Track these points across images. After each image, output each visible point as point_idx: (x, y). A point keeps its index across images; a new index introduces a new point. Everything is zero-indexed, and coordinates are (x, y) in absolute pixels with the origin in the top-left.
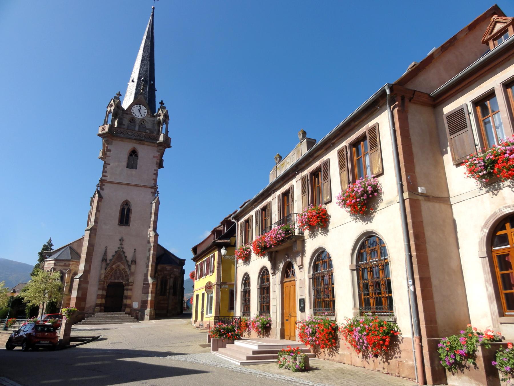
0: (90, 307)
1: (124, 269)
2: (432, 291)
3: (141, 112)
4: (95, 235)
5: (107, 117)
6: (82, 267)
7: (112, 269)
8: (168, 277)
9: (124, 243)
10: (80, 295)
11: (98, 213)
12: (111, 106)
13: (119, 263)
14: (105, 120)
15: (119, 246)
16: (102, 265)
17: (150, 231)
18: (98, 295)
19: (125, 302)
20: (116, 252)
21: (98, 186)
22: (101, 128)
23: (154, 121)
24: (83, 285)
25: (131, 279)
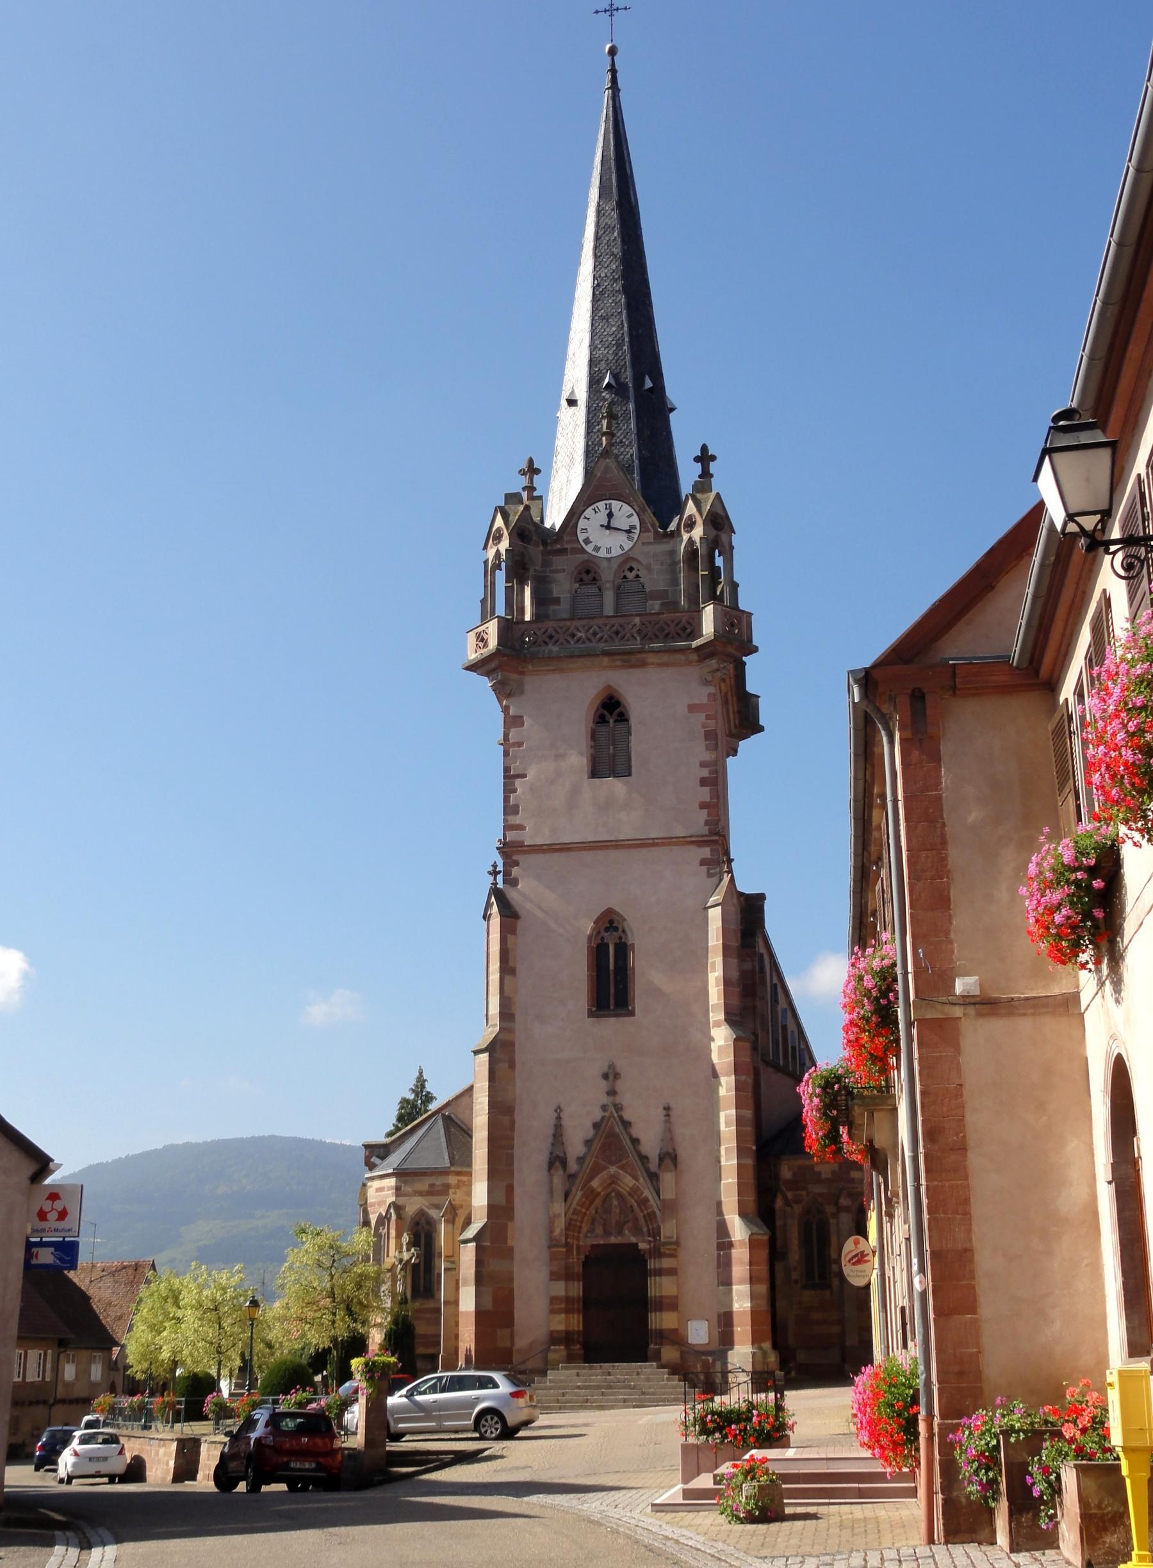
0: (531, 1345)
1: (634, 1191)
2: (973, 1287)
3: (612, 535)
4: (512, 1066)
5: (490, 587)
6: (480, 1194)
7: (591, 1195)
8: (829, 1209)
9: (620, 1086)
10: (488, 1305)
11: (508, 978)
12: (498, 538)
13: (613, 1169)
14: (484, 601)
15: (605, 1099)
16: (551, 1181)
17: (717, 1024)
18: (553, 1300)
19: (662, 1320)
20: (596, 1126)
21: (495, 873)
22: (472, 637)
23: (673, 553)
24: (494, 1265)
25: (668, 1230)
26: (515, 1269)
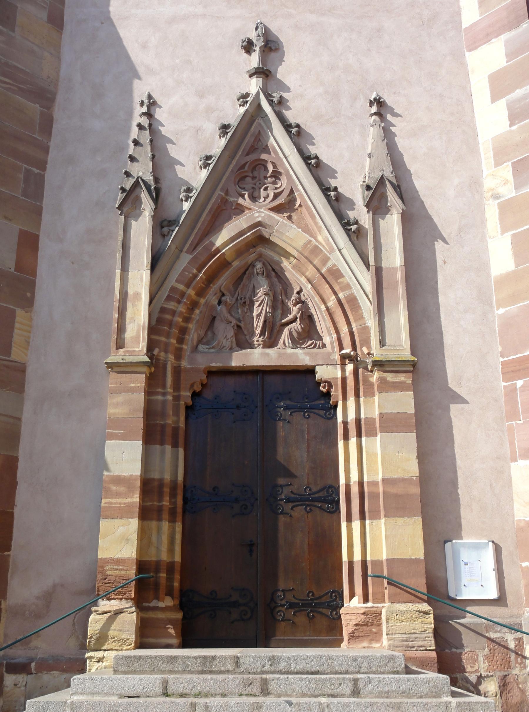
0: (48, 597)
26: (27, 415)
